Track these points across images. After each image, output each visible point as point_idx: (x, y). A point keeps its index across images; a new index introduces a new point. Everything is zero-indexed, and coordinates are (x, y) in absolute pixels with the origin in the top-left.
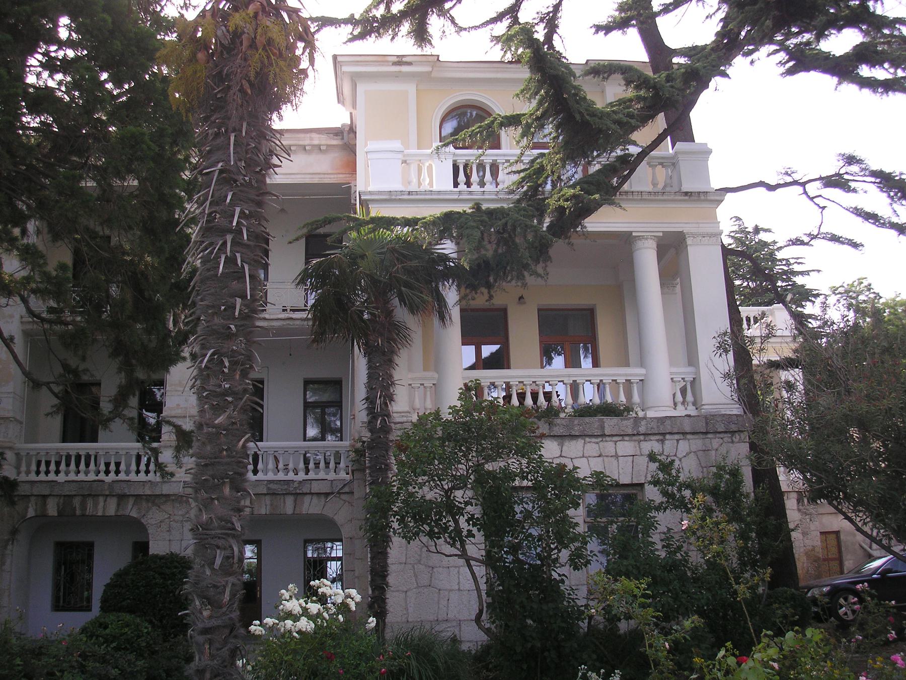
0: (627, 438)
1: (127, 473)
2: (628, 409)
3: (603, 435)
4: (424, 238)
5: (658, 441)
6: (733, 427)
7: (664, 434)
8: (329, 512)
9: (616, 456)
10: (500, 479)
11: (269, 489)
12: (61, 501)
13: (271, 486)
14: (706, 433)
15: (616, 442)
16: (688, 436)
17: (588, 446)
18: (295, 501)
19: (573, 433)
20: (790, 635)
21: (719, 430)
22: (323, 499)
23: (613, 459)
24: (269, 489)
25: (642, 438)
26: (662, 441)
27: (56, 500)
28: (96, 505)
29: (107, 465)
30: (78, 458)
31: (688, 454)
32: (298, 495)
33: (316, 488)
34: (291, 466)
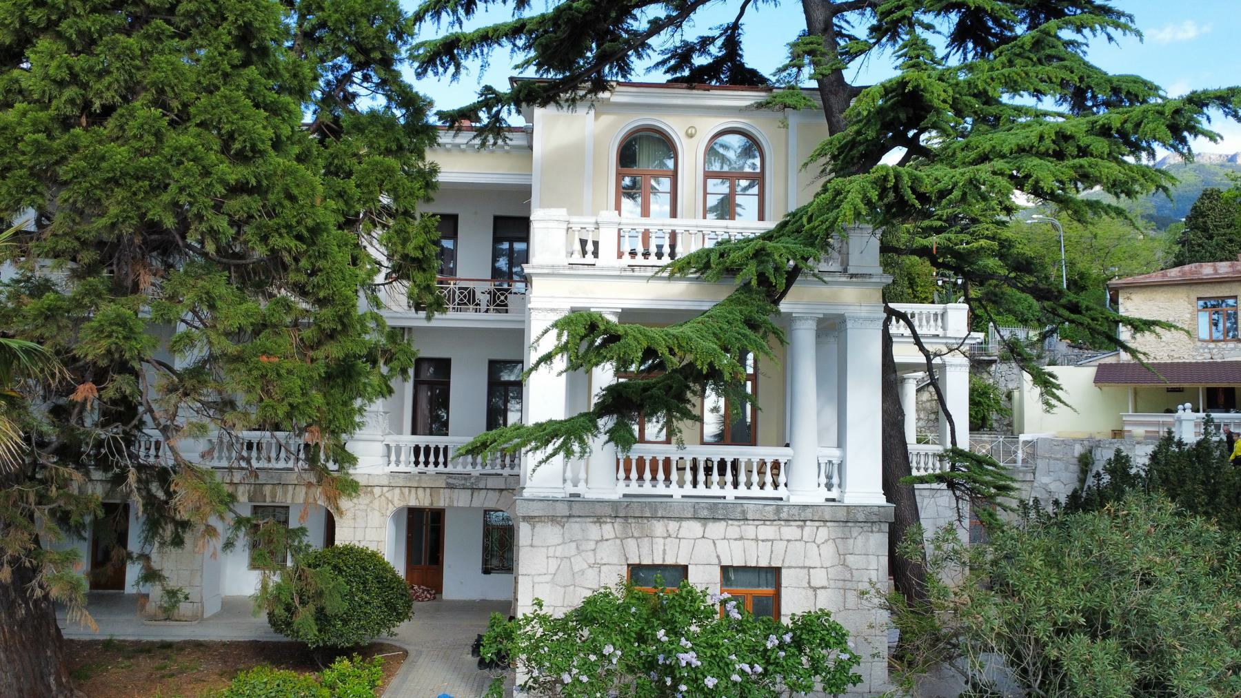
0: (768, 523)
1: (749, 485)
2: (91, 480)
4: (126, 274)
5: (798, 526)
6: (875, 518)
7: (805, 521)
9: (757, 540)
10: (159, 98)
12: (252, 489)
14: (847, 522)
15: (757, 526)
16: (828, 524)
17: (730, 528)
19: (716, 516)
21: (860, 520)
22: (497, 494)
23: (753, 542)
25: (782, 523)
26: (802, 527)
27: (247, 487)
28: (285, 493)
31: (826, 541)
34: (922, 465)
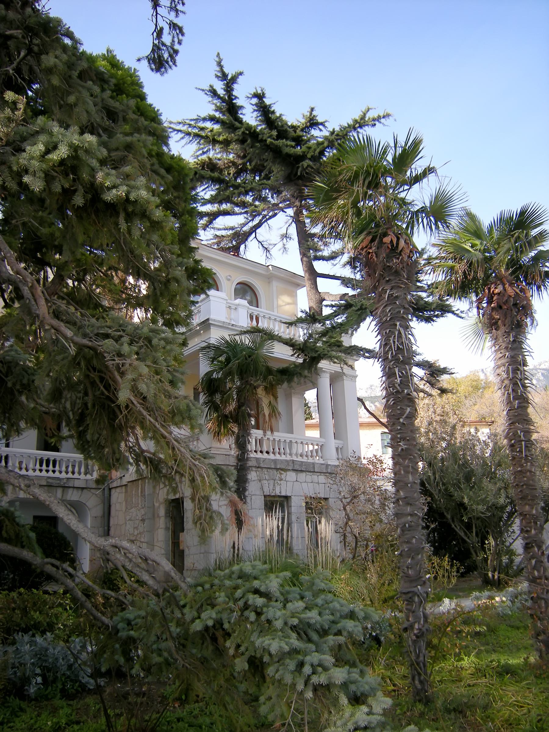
3: (314, 472)
8: (83, 500)
9: (318, 483)
11: (48, 482)
13: (49, 480)
18: (63, 491)
20: (48, 634)
24: (48, 482)
29: (67, 467)
30: (48, 462)
32: (65, 488)
33: (77, 484)
